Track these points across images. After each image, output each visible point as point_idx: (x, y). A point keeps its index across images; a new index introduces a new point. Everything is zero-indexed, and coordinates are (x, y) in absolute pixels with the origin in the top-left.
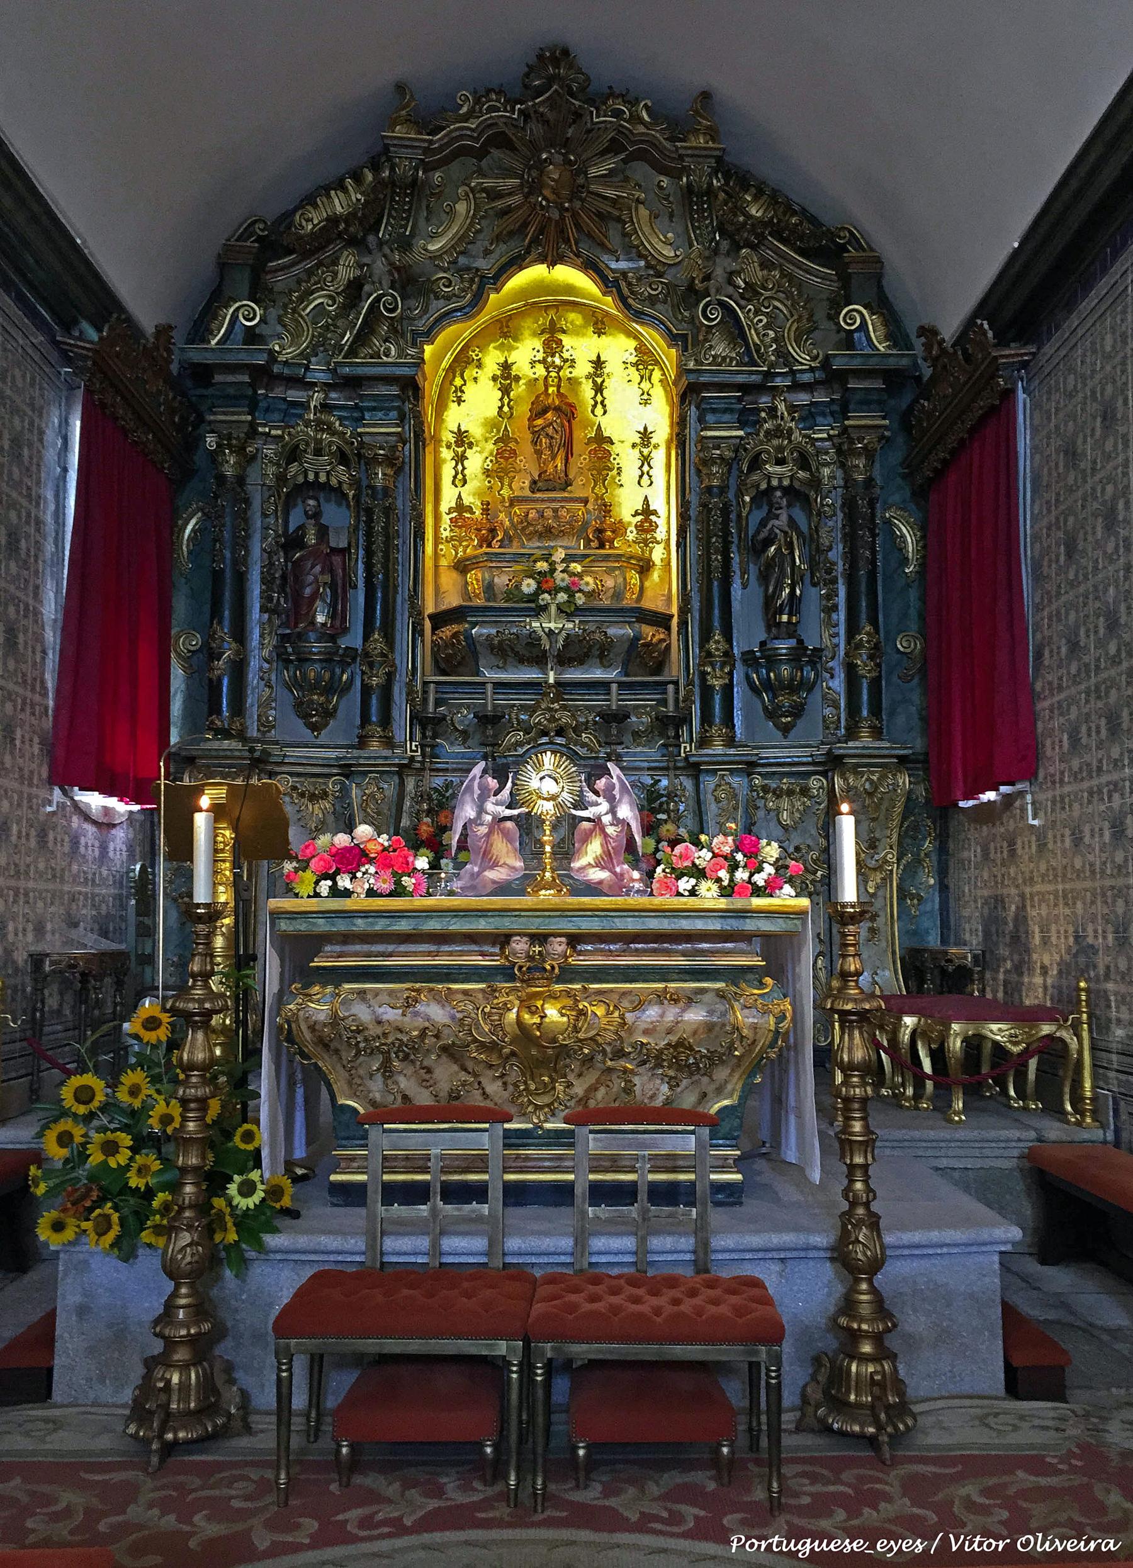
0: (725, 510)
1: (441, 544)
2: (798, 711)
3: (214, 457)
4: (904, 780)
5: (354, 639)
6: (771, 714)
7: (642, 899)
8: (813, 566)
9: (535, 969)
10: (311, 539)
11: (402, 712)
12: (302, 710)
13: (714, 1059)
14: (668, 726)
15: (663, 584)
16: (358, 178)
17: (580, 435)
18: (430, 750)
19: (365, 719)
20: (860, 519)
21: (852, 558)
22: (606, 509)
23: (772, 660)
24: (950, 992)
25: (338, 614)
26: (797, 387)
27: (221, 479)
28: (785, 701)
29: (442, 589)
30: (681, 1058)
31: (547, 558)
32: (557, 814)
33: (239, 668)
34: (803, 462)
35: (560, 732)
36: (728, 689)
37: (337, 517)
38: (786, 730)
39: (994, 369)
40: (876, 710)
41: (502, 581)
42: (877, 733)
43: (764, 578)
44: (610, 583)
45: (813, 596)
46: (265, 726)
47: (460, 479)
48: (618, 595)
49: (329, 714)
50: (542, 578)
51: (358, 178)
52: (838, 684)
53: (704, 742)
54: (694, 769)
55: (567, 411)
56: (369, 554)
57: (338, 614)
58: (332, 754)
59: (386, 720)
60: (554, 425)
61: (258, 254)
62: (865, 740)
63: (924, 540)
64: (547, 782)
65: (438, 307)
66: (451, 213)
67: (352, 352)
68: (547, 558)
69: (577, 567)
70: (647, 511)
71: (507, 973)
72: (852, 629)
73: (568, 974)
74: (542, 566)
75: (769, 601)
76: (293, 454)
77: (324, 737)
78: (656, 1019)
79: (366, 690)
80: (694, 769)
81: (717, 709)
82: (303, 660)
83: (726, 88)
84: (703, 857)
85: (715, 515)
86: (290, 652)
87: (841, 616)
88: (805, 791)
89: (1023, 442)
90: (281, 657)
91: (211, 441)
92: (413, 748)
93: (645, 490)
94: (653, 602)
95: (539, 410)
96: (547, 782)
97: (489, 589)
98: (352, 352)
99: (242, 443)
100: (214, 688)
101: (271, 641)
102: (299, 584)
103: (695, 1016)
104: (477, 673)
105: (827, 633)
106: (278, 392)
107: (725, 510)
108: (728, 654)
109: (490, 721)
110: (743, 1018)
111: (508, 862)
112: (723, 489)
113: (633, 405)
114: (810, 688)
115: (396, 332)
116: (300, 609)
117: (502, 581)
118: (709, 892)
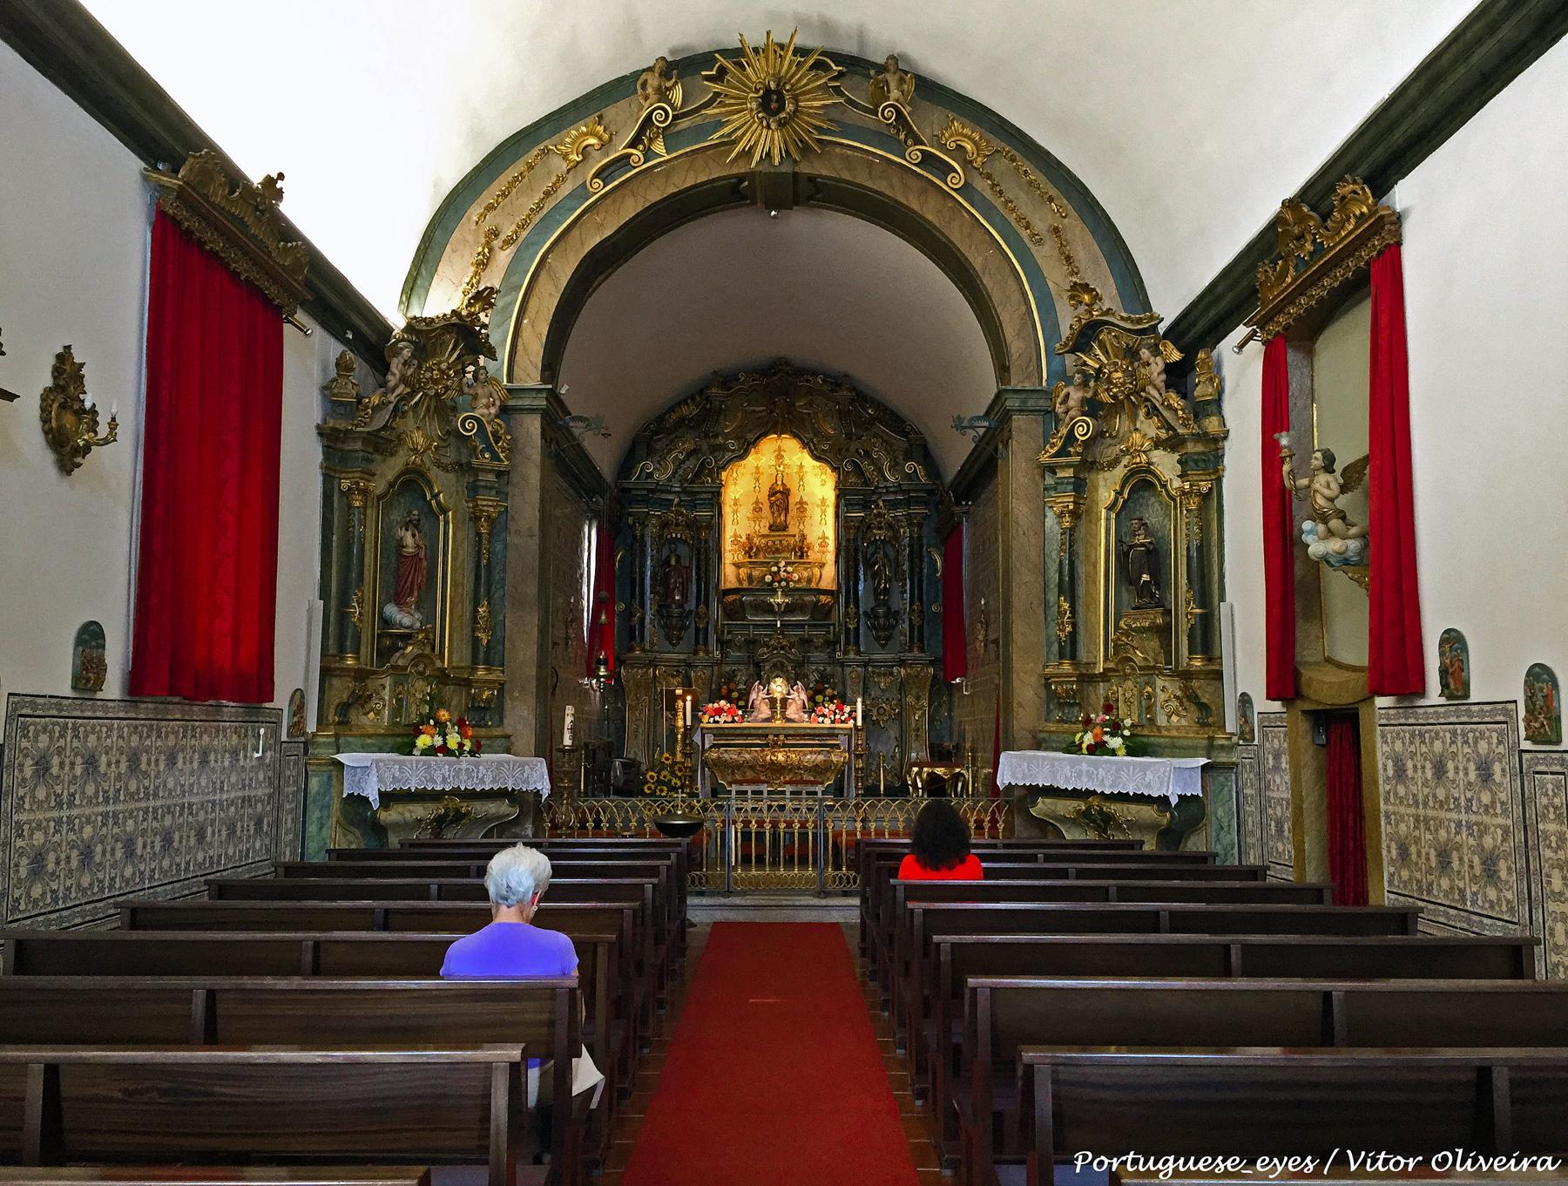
0: (856, 550)
1: (731, 555)
2: (888, 639)
3: (631, 527)
4: (931, 670)
5: (691, 605)
6: (877, 639)
7: (806, 722)
8: (896, 573)
9: (775, 744)
10: (673, 562)
11: (712, 638)
12: (669, 639)
13: (827, 770)
14: (832, 644)
15: (828, 576)
16: (693, 399)
17: (793, 500)
18: (724, 654)
19: (697, 639)
20: (916, 555)
21: (911, 569)
22: (803, 537)
23: (877, 617)
24: (103, 647)
25: (685, 596)
26: (888, 492)
27: (634, 537)
28: (882, 634)
29: (730, 575)
30: (817, 769)
31: (776, 564)
32: (780, 699)
33: (642, 620)
34: (890, 526)
35: (783, 648)
36: (857, 629)
37: (683, 550)
38: (883, 646)
39: (953, 515)
40: (921, 639)
41: (756, 573)
42: (922, 650)
43: (874, 578)
44: (806, 574)
45: (897, 585)
46: (652, 644)
47: (735, 522)
48: (809, 581)
49: (680, 639)
50: (774, 574)
51: (693, 399)
52: (906, 626)
53: (846, 652)
54: (842, 665)
55: (786, 493)
56: (698, 568)
57: (685, 596)
58: (682, 657)
59: (706, 643)
60: (780, 498)
61: (647, 439)
62: (916, 653)
63: (944, 562)
64: (778, 687)
65: (728, 455)
66: (735, 417)
67: (692, 481)
68: (776, 564)
69: (790, 569)
70: (824, 538)
71: (767, 745)
72: (912, 603)
73: (785, 745)
74: (775, 569)
75: (875, 590)
76: (665, 525)
77: (677, 648)
78: (811, 758)
79: (697, 629)
80: (842, 665)
81: (854, 638)
82: (670, 616)
83: (850, 372)
84: (826, 711)
85: (851, 549)
86: (663, 611)
87: (907, 596)
88: (891, 674)
89: (965, 543)
90: (659, 612)
91: (630, 520)
92: (717, 654)
93: (821, 527)
94: (824, 585)
95: (773, 493)
96: (778, 687)
97: (750, 577)
98: (692, 481)
99: (643, 520)
100: (632, 629)
101: (655, 607)
102: (667, 580)
103: (821, 757)
104: (744, 619)
105: (902, 601)
106: (657, 495)
107: (856, 550)
108: (857, 614)
109: (752, 643)
110: (834, 759)
111: (765, 711)
112: (855, 540)
113: (818, 486)
114: (894, 627)
115: (710, 474)
116: (668, 594)
117: (756, 573)
118: (827, 721)
